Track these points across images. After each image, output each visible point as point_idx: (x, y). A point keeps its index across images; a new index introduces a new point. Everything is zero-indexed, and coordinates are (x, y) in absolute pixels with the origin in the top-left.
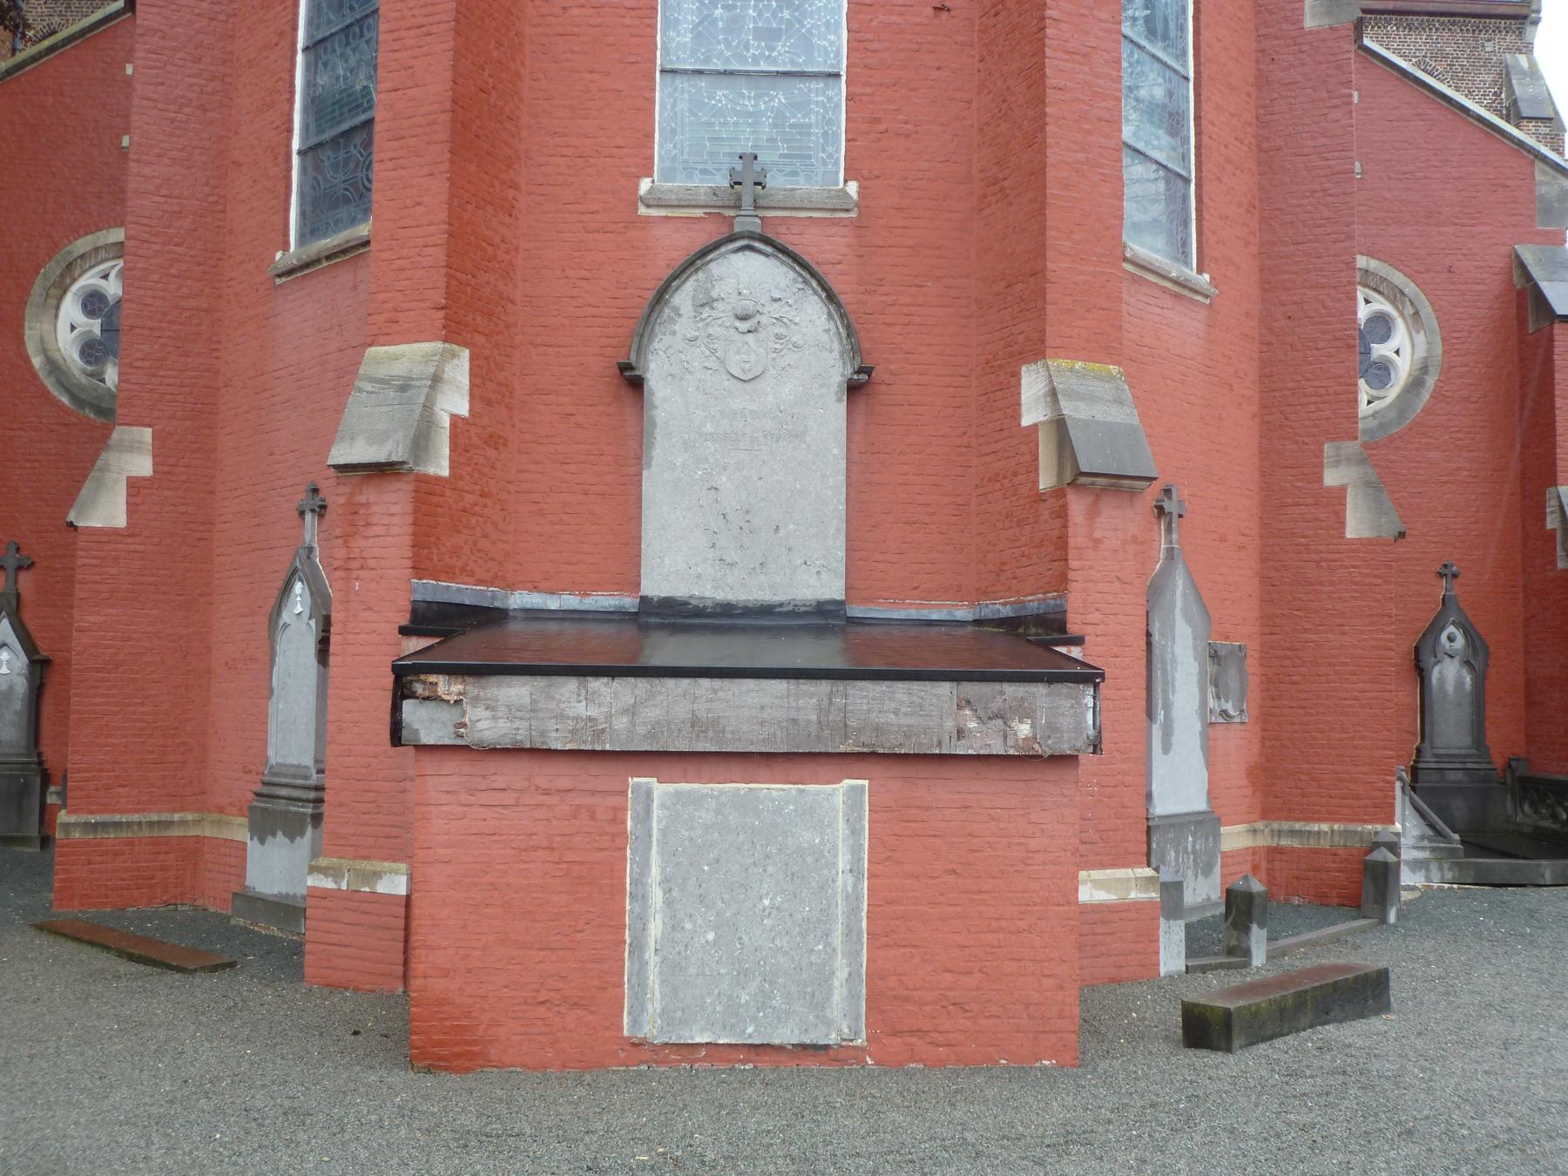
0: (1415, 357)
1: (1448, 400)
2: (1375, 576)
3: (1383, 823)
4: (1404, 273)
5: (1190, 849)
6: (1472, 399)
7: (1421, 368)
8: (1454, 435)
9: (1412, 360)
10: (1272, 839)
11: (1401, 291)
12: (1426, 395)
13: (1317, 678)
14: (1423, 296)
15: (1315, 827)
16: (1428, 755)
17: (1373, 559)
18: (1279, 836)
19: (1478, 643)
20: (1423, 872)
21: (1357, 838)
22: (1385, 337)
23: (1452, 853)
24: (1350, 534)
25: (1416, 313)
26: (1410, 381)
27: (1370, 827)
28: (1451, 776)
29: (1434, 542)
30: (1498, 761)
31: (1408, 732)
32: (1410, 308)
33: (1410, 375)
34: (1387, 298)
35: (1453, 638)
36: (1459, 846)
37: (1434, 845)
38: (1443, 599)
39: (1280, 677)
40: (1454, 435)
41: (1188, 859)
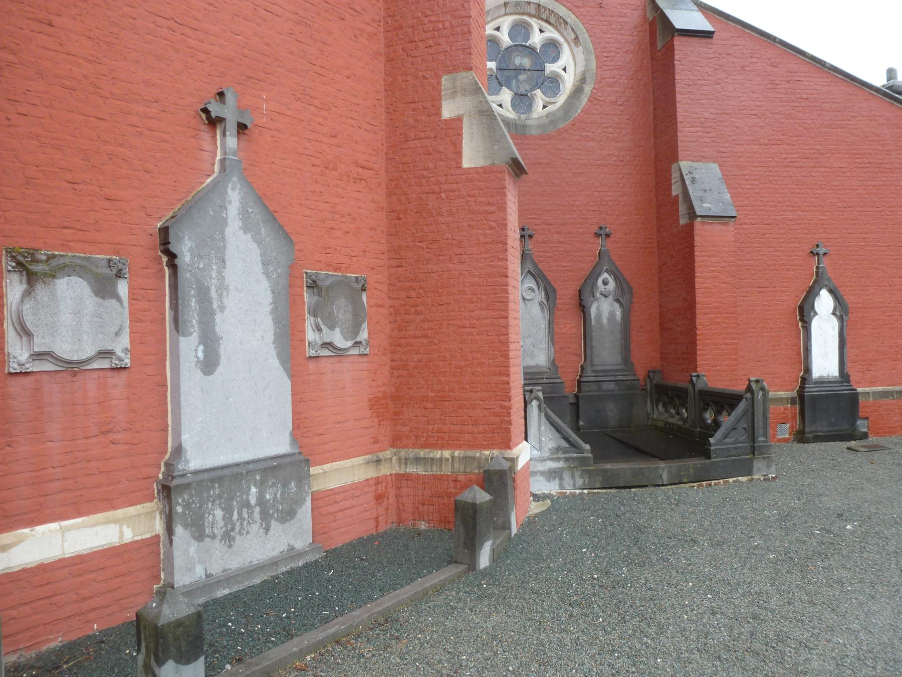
0: (577, 71)
1: (601, 103)
2: (489, 204)
3: (500, 448)
4: (566, 7)
5: (253, 501)
6: (618, 103)
7: (581, 80)
8: (605, 130)
9: (575, 74)
10: (400, 467)
11: (565, 21)
12: (585, 100)
13: (439, 308)
14: (581, 25)
15: (438, 454)
16: (589, 372)
17: (488, 188)
18: (406, 464)
19: (625, 286)
20: (557, 481)
21: (476, 464)
22: (555, 59)
23: (583, 461)
24: (466, 164)
25: (577, 38)
26: (573, 90)
27: (487, 453)
28: (605, 386)
29: (592, 211)
30: (641, 374)
31: (575, 354)
32: (572, 34)
33: (574, 85)
34: (555, 27)
35: (606, 283)
36: (590, 455)
37: (567, 455)
38: (599, 253)
39: (406, 308)
40: (605, 130)
41: (251, 515)
